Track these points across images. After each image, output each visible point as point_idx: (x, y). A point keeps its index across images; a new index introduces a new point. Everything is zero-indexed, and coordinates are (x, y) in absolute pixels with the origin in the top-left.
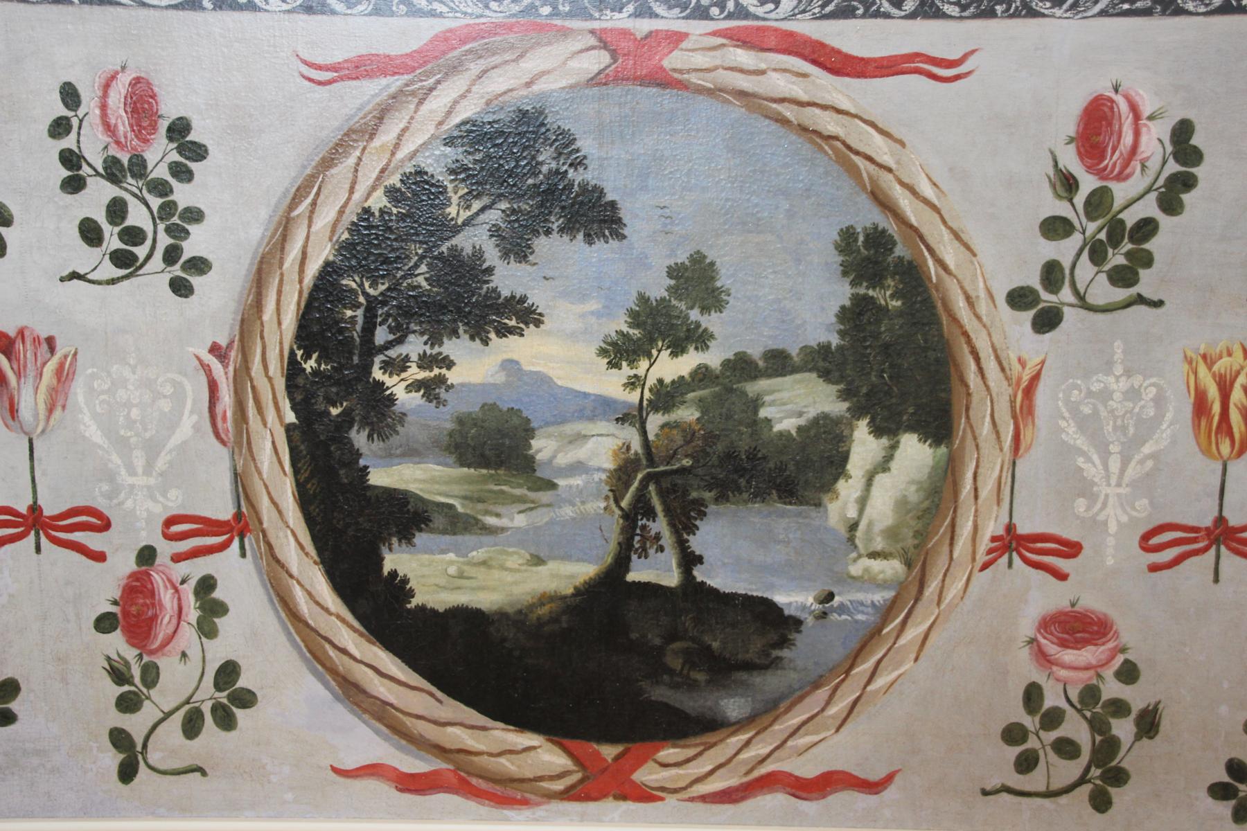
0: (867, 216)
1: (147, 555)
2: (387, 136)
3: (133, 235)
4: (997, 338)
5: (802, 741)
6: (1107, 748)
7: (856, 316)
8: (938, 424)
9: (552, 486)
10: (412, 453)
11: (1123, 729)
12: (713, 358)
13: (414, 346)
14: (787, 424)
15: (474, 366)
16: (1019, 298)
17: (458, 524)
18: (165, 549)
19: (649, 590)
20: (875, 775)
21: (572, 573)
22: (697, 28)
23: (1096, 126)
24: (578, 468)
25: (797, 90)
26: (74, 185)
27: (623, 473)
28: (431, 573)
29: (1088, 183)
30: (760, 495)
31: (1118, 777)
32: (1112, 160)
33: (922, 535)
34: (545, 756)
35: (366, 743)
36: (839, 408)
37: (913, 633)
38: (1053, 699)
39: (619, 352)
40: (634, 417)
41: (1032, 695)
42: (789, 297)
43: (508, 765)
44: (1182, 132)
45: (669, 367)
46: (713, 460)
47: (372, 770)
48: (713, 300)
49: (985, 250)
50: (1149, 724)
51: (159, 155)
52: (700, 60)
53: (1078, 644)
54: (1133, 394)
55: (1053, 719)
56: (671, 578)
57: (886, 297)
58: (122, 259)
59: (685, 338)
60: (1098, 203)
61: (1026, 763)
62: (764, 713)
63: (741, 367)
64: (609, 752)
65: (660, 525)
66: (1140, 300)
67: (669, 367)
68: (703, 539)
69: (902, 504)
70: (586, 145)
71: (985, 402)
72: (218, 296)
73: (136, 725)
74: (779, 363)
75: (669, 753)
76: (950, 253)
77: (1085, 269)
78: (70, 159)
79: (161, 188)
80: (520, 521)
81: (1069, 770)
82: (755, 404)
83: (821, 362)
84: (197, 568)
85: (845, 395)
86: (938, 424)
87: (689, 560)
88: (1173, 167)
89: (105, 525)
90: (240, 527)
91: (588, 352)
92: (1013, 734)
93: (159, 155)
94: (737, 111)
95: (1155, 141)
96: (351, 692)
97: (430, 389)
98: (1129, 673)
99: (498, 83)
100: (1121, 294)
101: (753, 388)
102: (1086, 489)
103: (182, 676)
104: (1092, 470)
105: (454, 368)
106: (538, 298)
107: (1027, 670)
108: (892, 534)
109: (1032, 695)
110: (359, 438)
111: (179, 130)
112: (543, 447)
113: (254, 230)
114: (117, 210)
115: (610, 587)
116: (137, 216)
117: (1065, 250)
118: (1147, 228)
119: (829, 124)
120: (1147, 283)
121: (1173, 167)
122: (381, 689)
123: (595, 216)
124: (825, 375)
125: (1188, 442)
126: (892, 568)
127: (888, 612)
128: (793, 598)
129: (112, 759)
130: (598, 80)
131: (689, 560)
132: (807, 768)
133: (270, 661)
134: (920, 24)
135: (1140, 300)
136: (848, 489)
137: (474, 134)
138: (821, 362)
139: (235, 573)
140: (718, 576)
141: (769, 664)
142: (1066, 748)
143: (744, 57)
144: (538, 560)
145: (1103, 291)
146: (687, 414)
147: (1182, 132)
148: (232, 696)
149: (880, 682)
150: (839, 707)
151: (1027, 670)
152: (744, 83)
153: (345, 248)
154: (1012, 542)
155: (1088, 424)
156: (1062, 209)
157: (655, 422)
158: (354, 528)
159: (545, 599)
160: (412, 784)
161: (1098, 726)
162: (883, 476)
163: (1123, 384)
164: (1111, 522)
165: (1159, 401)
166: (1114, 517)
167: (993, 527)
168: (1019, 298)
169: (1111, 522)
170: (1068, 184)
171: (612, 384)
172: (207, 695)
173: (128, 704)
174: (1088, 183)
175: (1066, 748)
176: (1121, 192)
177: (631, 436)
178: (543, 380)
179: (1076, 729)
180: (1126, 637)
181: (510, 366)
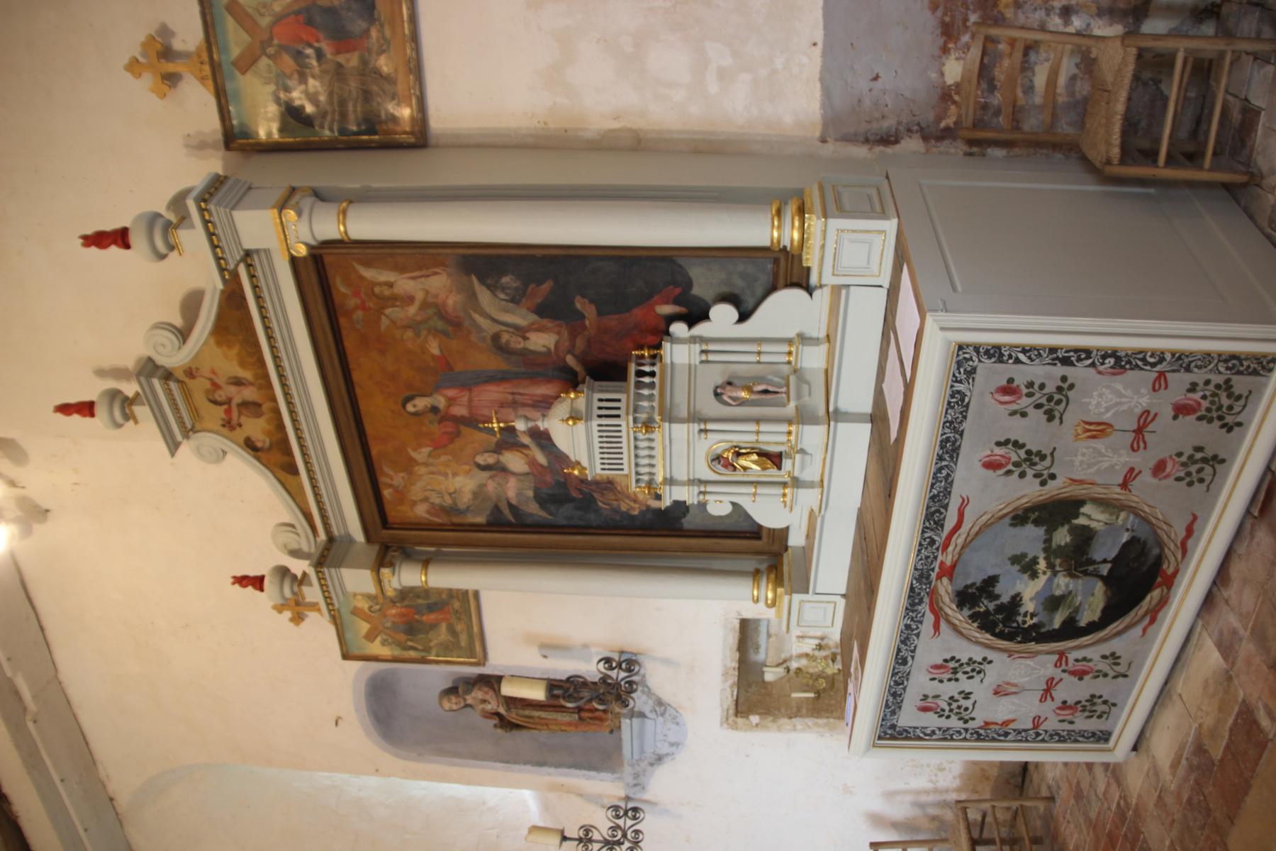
0: (1007, 520)
1: (1064, 671)
2: (957, 622)
3: (973, 670)
4: (1054, 489)
5: (1173, 536)
6: (1204, 460)
7: (1037, 523)
8: (1080, 503)
9: (1070, 592)
10: (1051, 620)
11: (1199, 456)
12: (1042, 556)
13: (1020, 619)
14: (1068, 539)
15: (1029, 606)
16: (1043, 483)
17: (1077, 610)
18: (1064, 667)
19: (1110, 571)
20: (1191, 518)
21: (1099, 588)
22: (940, 558)
23: (991, 465)
24: (1067, 586)
25: (964, 537)
26: (957, 680)
27: (1071, 575)
28: (1091, 612)
29: (1010, 467)
30: (1089, 545)
31: (1215, 457)
32: (1003, 461)
33: (1114, 506)
34: (1156, 594)
35: (1138, 631)
36: (1066, 527)
37: (1147, 509)
38: (1182, 474)
39: (1034, 575)
40: (1055, 574)
41: (1178, 479)
42: (1030, 539)
43: (1154, 602)
44: (998, 444)
45: (1042, 565)
46: (1077, 558)
47: (1145, 630)
48: (1024, 555)
49: (1028, 491)
50: (1199, 449)
51: (952, 664)
52: (950, 557)
53: (1165, 467)
54: (1083, 455)
55: (1189, 474)
56: (1109, 566)
57: (1033, 516)
58: (979, 672)
59: (1035, 561)
60: (1017, 464)
61: (1201, 481)
62: (1161, 544)
63: (1045, 550)
64: (1159, 579)
65: (1091, 568)
66: (1052, 454)
67: (1042, 565)
68: (1098, 556)
69: (1102, 512)
70: (969, 582)
71: (1078, 491)
72: (991, 655)
73: (1111, 674)
74: (1048, 541)
75: (1165, 566)
76: (1025, 500)
77: (1038, 467)
78: (950, 680)
79: (962, 665)
80: (1079, 598)
81: (1208, 470)
82: (1059, 546)
83: (1050, 532)
84: (1071, 662)
85: (1062, 525)
86: (1080, 503)
87: (1105, 561)
88: (1010, 446)
89: (1148, 412)
90: (1062, 654)
91: (1032, 583)
92: (1190, 484)
93: (952, 664)
94: (967, 550)
95: (1000, 451)
96: (1119, 633)
97: (1033, 615)
98: (1180, 454)
99: (947, 600)
100: (1049, 459)
101: (1054, 545)
102: (1112, 467)
103: (1104, 666)
104: (1106, 465)
105: (171, 26)
106: (1013, 593)
107: (1170, 481)
108: (1111, 514)
109: (1178, 479)
110: (1043, 630)
111: (946, 661)
112: (1058, 593)
113: (978, 649)
114: (965, 673)
115: (1105, 580)
116: (968, 669)
117: (1030, 472)
118: (1029, 453)
119: (976, 529)
120: (1047, 451)
121: (1010, 446)
122: (1121, 627)
123: (992, 581)
124: (1055, 529)
125: (1106, 440)
126: (1123, 515)
127: (1137, 515)
128: (1125, 537)
129: (1120, 679)
130: (951, 580)
131: (1105, 561)
132: (1183, 534)
133: (1106, 648)
134: (950, 508)
135: (1052, 454)
136: (1093, 525)
137: (960, 605)
138: (1050, 532)
139: (1072, 656)
140: (1113, 554)
141: (1145, 543)
142: (1200, 471)
143: (950, 549)
144: (1093, 594)
145: (1047, 463)
146: (1058, 561)
147: (998, 444)
148: (1114, 657)
149: (1160, 517)
150: (1165, 527)
151: (1170, 481)
152: (958, 548)
153: (987, 631)
154: (1124, 485)
155: (1090, 466)
156: (1016, 474)
157: (1058, 568)
158: (1071, 630)
159: (1105, 593)
160: (1153, 621)
161: (1196, 462)
162: (1092, 517)
163: (1080, 458)
164: (1125, 458)
165: (1088, 448)
166: (1124, 458)
167: (1118, 490)
168: (1043, 483)
169: (1125, 458)
170: (1009, 473)
171: (1042, 579)
172: (1110, 661)
173: (1106, 675)
174: (1010, 467)
175: (1200, 471)
176: (1014, 458)
177: (1060, 575)
178: (1037, 593)
179: (1193, 469)
180: (1166, 455)
181: (1031, 599)
